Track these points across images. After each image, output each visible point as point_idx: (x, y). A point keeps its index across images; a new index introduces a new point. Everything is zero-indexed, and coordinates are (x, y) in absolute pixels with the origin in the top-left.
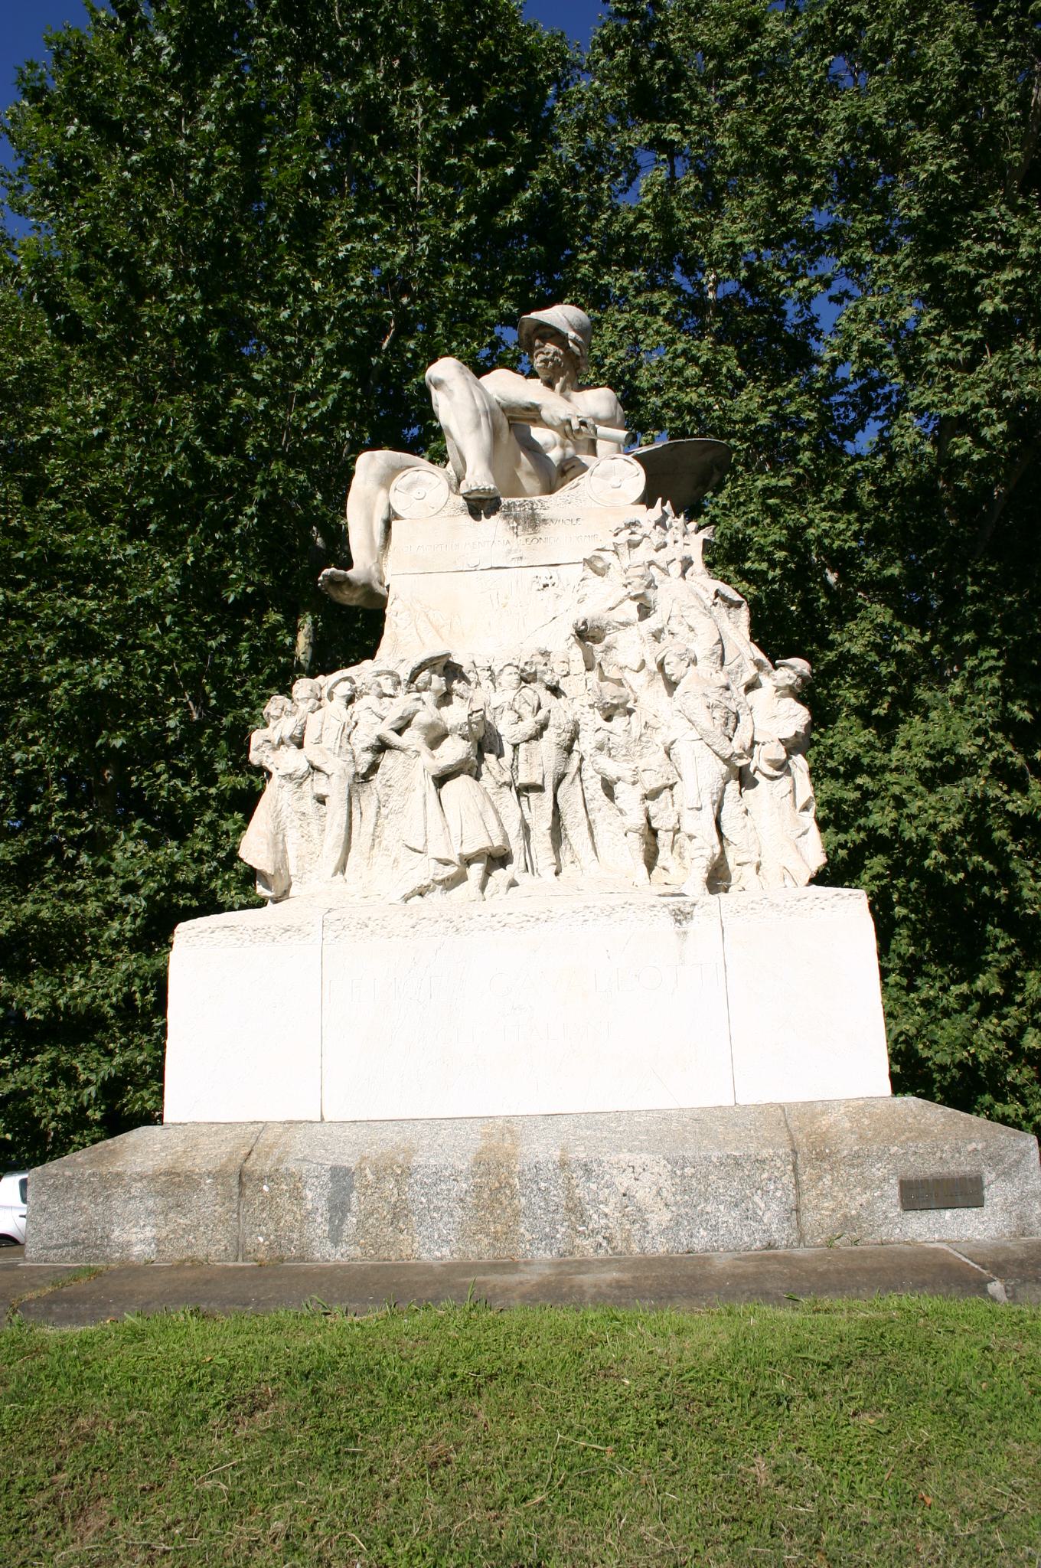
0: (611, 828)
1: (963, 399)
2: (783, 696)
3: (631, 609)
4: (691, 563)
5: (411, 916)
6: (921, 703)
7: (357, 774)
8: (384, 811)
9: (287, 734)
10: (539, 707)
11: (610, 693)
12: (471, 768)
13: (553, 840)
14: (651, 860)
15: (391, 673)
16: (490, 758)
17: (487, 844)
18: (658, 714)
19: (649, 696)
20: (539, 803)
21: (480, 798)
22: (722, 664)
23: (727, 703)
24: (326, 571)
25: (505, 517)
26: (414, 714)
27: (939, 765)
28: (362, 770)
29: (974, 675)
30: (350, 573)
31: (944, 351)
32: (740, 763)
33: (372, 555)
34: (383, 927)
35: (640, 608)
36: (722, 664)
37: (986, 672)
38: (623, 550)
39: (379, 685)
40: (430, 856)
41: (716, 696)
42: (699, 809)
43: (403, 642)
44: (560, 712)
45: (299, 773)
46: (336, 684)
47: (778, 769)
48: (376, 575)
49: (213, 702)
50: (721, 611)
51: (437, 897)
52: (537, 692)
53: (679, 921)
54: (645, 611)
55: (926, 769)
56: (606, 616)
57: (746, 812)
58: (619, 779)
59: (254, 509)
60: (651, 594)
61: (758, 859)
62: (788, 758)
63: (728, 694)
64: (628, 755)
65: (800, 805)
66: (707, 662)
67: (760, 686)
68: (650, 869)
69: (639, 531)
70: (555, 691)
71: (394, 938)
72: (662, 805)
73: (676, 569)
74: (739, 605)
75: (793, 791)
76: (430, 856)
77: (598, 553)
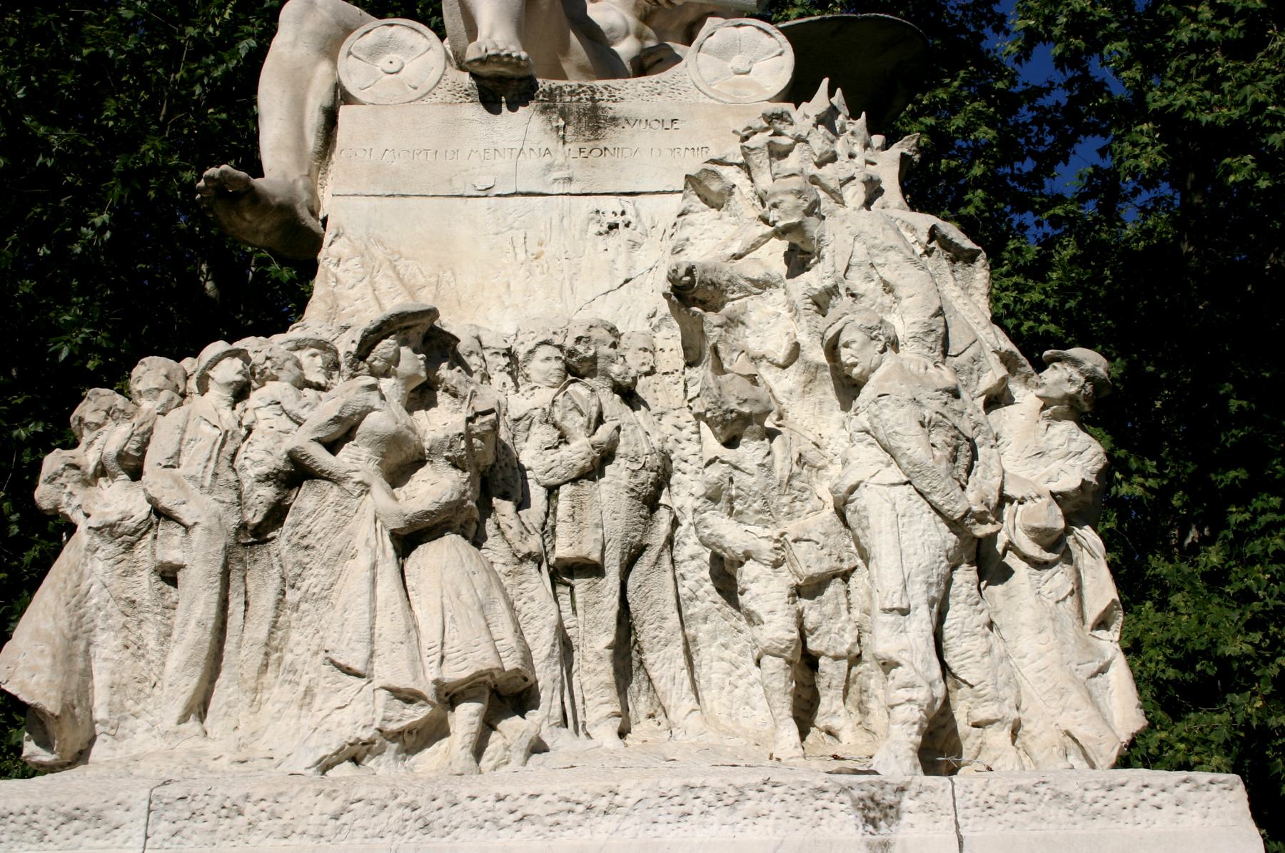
0: (727, 654)
1: (1239, 97)
2: (1056, 417)
3: (773, 255)
4: (880, 192)
5: (332, 795)
6: (1158, 582)
7: (243, 527)
8: (292, 596)
9: (112, 449)
10: (600, 420)
11: (735, 395)
12: (463, 521)
13: (617, 671)
14: (805, 711)
15: (323, 346)
16: (505, 507)
17: (491, 663)
18: (824, 442)
19: (811, 415)
20: (593, 597)
21: (480, 579)
22: (945, 353)
23: (957, 421)
24: (212, 171)
25: (544, 110)
26: (363, 414)
27: (1189, 676)
28: (254, 517)
29: (1243, 534)
30: (258, 182)
31: (1204, 29)
32: (981, 530)
34: (274, 816)
35: (788, 257)
36: (945, 353)
37: (1261, 533)
38: (760, 160)
39: (298, 365)
40: (377, 683)
41: (936, 405)
42: (905, 612)
43: (347, 295)
45: (130, 524)
46: (215, 362)
47: (1048, 549)
48: (305, 197)
50: (939, 262)
51: (384, 766)
53: (873, 822)
54: (800, 259)
55: (1168, 681)
56: (727, 267)
57: (991, 625)
58: (748, 556)
59: (106, 216)
60: (812, 224)
61: (1014, 714)
62: (1067, 531)
63: (957, 405)
64: (768, 513)
65: (1091, 617)
67: (1011, 401)
68: (803, 734)
70: (629, 395)
71: (295, 839)
72: (828, 609)
73: (855, 194)
74: (970, 258)
75: (1078, 591)
76: (377, 683)
77: (711, 167)
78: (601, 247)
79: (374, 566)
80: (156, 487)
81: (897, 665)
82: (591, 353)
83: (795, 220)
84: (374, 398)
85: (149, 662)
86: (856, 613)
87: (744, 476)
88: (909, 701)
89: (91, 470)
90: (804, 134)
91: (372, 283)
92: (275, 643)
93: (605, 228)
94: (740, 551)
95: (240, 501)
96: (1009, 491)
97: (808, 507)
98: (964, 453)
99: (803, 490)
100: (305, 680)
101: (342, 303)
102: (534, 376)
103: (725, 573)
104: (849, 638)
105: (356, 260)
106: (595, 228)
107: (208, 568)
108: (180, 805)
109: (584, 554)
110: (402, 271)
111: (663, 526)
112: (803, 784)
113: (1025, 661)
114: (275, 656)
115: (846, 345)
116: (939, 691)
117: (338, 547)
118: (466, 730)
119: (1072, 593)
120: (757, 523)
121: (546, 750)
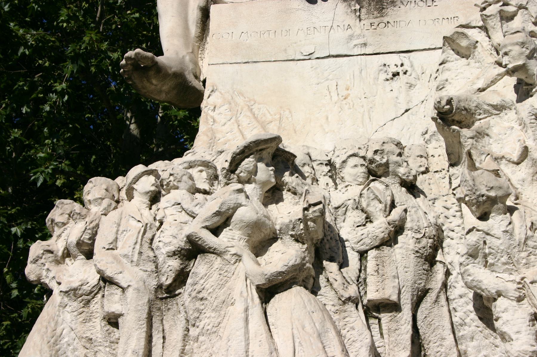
3: (506, 88)
7: (160, 287)
8: (193, 332)
9: (73, 239)
10: (393, 205)
11: (485, 184)
12: (304, 277)
15: (207, 165)
16: (331, 267)
20: (394, 326)
21: (317, 316)
24: (130, 53)
30: (159, 59)
33: (186, 45)
35: (517, 88)
38: (494, 23)
39: (191, 178)
43: (220, 131)
44: (420, 214)
48: (191, 66)
49: (15, 293)
52: (386, 188)
56: (475, 97)
58: (499, 294)
59: (64, 85)
64: (511, 264)
70: (411, 187)
79: (246, 310)
82: (384, 160)
84: (241, 198)
87: (494, 240)
89: (60, 253)
90: (524, 3)
91: (237, 121)
93: (390, 75)
101: (218, 136)
105: (226, 107)
106: (383, 76)
109: (386, 296)
110: (256, 113)
117: (222, 298)
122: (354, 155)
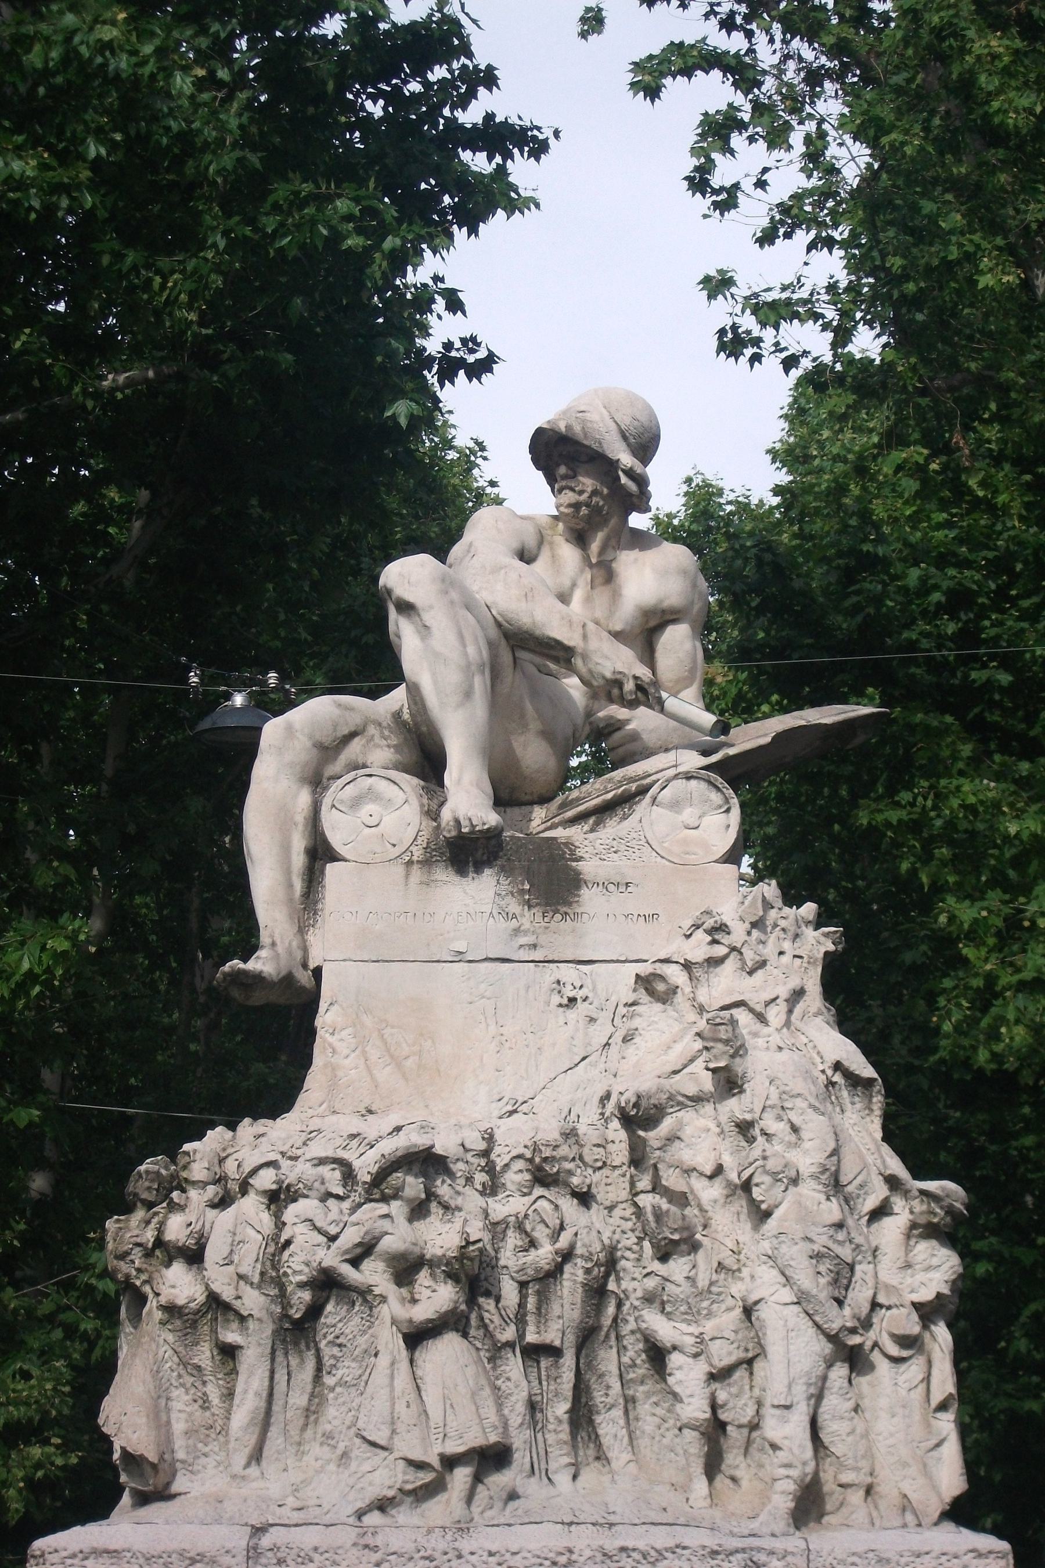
10: (562, 1228)
14: (712, 1467)
19: (726, 1227)
42: (787, 1407)
51: (403, 1515)
58: (675, 1348)
61: (869, 1480)
63: (841, 1236)
64: (692, 1315)
66: (813, 1184)
69: (726, 940)
75: (927, 1379)
76: (396, 1454)
78: (561, 1021)
79: (393, 1364)
80: (217, 1284)
81: (780, 1449)
82: (555, 1170)
83: (722, 1064)
84: (386, 1225)
85: (213, 1415)
86: (757, 1392)
87: (673, 1287)
88: (788, 1477)
89: (150, 1245)
90: (739, 945)
91: (364, 1052)
92: (313, 1408)
93: (565, 1001)
94: (669, 1345)
95: (286, 1305)
96: (881, 1299)
97: (723, 1307)
98: (842, 1276)
99: (719, 1294)
100: (341, 1446)
101: (340, 1074)
102: (509, 1185)
103: (657, 1355)
104: (750, 1411)
105: (350, 1030)
106: (556, 999)
107: (259, 1350)
108: (270, 1554)
109: (548, 1341)
110: (389, 1040)
111: (611, 1310)
112: (704, 1547)
113: (880, 1438)
114: (312, 1418)
115: (757, 1185)
116: (810, 1468)
117: (364, 1346)
118: (462, 1487)
119: (922, 1381)
120: (684, 1321)
121: (518, 1497)
122: (519, 1157)
